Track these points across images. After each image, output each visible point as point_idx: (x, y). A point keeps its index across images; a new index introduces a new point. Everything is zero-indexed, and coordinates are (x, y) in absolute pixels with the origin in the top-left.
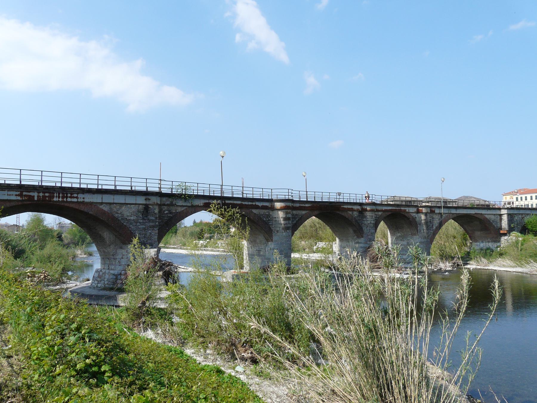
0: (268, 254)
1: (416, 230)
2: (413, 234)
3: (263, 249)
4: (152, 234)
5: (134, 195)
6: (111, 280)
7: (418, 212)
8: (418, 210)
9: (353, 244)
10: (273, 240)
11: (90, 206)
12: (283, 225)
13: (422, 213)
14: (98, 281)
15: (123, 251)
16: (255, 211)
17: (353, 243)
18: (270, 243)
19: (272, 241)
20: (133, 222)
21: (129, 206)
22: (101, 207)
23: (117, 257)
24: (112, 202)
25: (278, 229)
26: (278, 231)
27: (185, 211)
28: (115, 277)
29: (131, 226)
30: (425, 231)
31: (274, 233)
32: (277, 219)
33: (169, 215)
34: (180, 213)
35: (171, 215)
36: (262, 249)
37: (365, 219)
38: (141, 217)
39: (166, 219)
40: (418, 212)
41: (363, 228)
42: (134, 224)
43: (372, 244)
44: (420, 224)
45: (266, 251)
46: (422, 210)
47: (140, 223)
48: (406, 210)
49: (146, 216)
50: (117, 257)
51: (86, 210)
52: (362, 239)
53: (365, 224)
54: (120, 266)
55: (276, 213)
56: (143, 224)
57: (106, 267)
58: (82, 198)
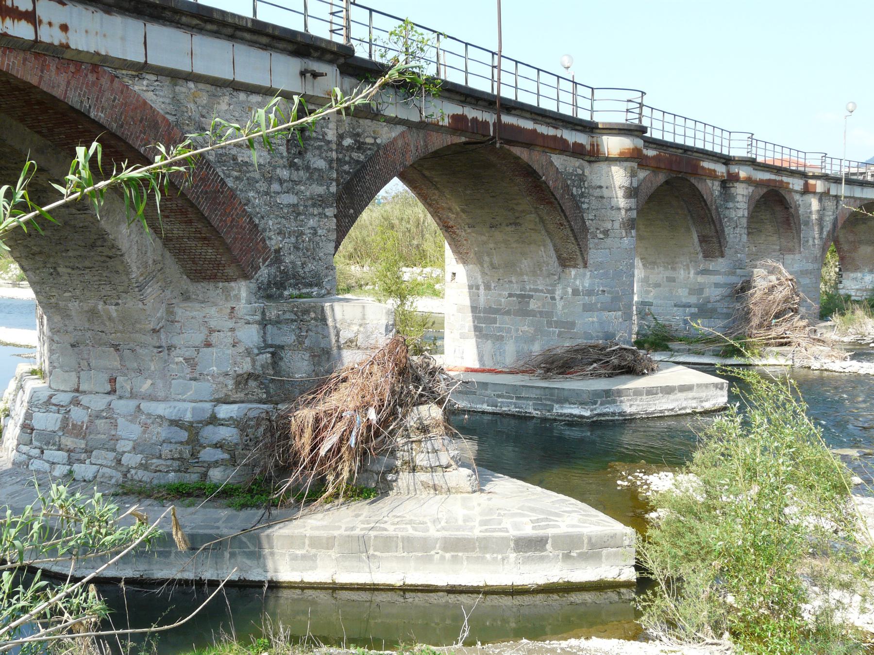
0: (564, 307)
1: (796, 240)
2: (784, 251)
3: (542, 291)
4: (320, 232)
5: (265, 47)
6: (166, 450)
7: (807, 191)
8: (806, 185)
9: (692, 275)
10: (590, 262)
11: (91, 78)
12: (623, 212)
13: (814, 193)
14: (69, 451)
15: (213, 311)
16: (558, 160)
17: (692, 272)
18: (573, 272)
19: (585, 266)
20: (257, 175)
21: (242, 96)
22: (136, 88)
23: (177, 340)
24: (184, 66)
25: (608, 225)
26: (606, 233)
27: (400, 143)
28: (184, 435)
29: (251, 194)
30: (816, 241)
31: (595, 237)
32: (606, 193)
33: (355, 155)
34: (385, 147)
35: (362, 158)
36: (536, 290)
37: (731, 205)
38: (285, 154)
39: (348, 173)
40: (807, 191)
41: (726, 229)
42: (262, 186)
43: (751, 275)
44: (807, 223)
45: (553, 298)
46: (815, 185)
47: (281, 181)
48: (789, 183)
49: (300, 153)
50: (177, 340)
51: (74, 99)
52: (720, 260)
53: (730, 219)
54: (195, 379)
55: (604, 172)
56: (291, 186)
57: (96, 381)
58: (57, 22)
